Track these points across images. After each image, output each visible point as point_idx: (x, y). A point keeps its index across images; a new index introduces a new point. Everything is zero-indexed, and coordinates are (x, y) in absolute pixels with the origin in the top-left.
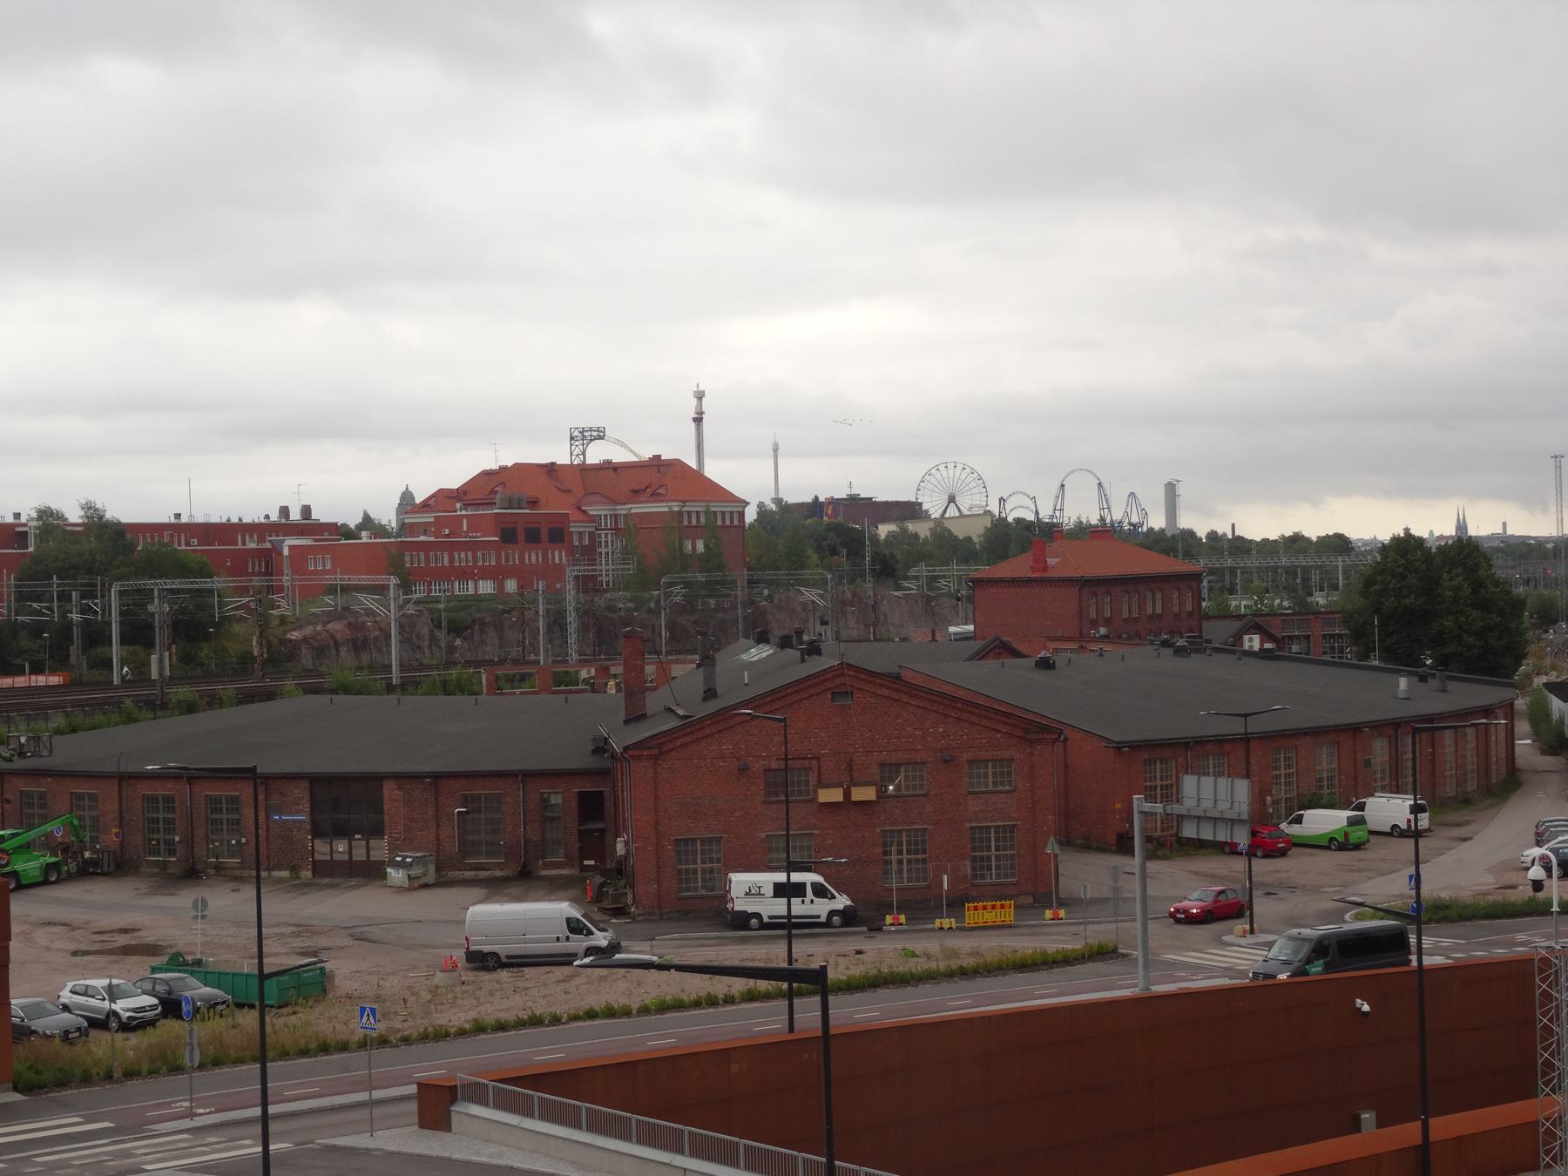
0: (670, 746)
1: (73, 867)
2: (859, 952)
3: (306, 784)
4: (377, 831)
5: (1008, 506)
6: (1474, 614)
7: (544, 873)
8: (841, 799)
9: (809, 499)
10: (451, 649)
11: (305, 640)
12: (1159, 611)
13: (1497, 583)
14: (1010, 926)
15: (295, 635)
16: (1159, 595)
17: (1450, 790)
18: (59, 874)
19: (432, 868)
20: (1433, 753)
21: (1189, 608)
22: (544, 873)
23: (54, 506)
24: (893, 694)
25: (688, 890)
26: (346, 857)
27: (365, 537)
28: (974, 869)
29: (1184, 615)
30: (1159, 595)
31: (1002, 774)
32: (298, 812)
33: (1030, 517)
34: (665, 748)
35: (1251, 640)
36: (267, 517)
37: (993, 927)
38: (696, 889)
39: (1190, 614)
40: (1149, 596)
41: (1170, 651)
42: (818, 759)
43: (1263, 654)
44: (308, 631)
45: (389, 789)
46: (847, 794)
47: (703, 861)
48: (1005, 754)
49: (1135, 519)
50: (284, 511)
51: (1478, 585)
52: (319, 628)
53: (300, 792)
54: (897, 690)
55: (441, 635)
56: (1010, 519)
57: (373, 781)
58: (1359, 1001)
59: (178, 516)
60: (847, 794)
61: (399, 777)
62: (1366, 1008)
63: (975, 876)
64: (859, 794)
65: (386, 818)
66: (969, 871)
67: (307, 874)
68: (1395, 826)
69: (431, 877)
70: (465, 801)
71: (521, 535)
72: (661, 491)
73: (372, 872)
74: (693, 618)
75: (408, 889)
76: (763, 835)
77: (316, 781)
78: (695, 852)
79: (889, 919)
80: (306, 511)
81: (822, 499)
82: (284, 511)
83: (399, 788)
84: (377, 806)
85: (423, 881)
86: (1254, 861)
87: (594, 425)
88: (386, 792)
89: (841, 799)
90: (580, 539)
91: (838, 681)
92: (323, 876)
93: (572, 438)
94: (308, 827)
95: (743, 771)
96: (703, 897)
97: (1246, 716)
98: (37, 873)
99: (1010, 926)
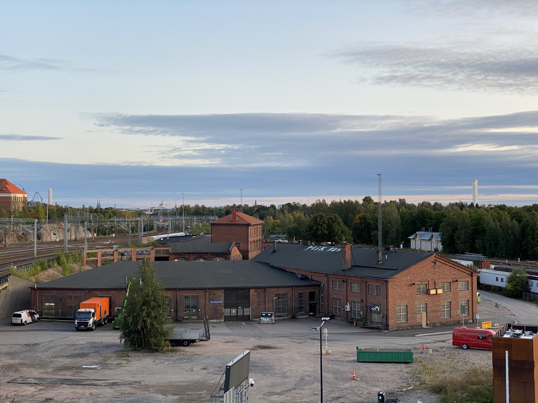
3: (223, 291)
32: (220, 300)
45: (252, 292)
53: (221, 294)
70: (277, 295)
83: (256, 291)
84: (248, 297)
88: (251, 293)
94: (223, 305)
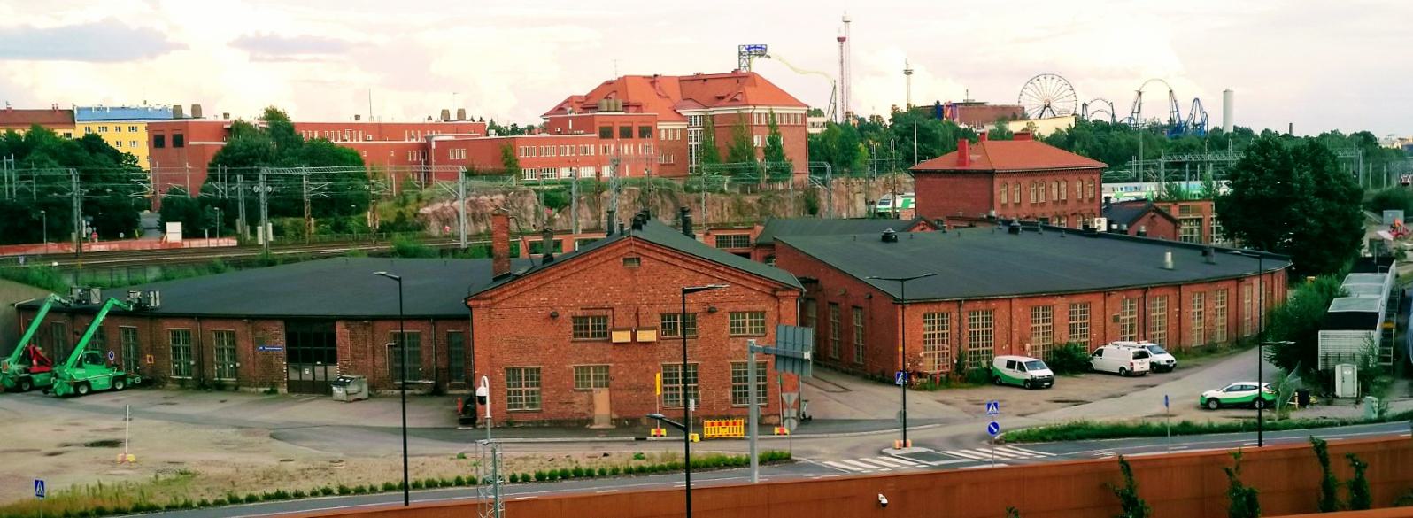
0: (500, 298)
1: (138, 380)
2: (605, 455)
4: (331, 359)
5: (1090, 109)
6: (1317, 201)
7: (450, 392)
8: (630, 340)
9: (933, 104)
10: (551, 220)
11: (435, 213)
12: (1042, 200)
13: (1340, 177)
14: (741, 439)
15: (427, 210)
16: (1063, 185)
17: (1197, 341)
18: (125, 384)
19: (365, 387)
20: (1180, 312)
21: (1091, 195)
22: (450, 392)
23: (279, 109)
24: (670, 260)
25: (515, 406)
26: (311, 378)
27: (493, 135)
28: (735, 395)
29: (1086, 201)
30: (1063, 185)
31: (757, 323)
33: (1107, 119)
34: (497, 300)
35: (1099, 222)
36: (430, 118)
37: (716, 439)
38: (521, 406)
39: (1091, 200)
40: (1055, 185)
41: (1006, 228)
42: (612, 309)
43: (1109, 235)
44: (438, 206)
46: (634, 336)
47: (527, 385)
48: (758, 307)
49: (1198, 120)
50: (445, 114)
51: (1322, 178)
52: (447, 204)
54: (673, 257)
55: (544, 209)
56: (1091, 120)
57: (330, 321)
58: (881, 495)
59: (358, 117)
60: (634, 336)
61: (348, 319)
62: (884, 501)
63: (735, 401)
64: (644, 336)
65: (338, 349)
66: (730, 397)
67: (283, 390)
68: (1122, 369)
69: (365, 394)
71: (616, 132)
72: (738, 97)
73: (322, 389)
74: (758, 197)
75: (347, 402)
76: (571, 366)
77: (289, 321)
78: (520, 378)
79: (653, 432)
80: (461, 114)
81: (942, 104)
82: (445, 114)
83: (347, 327)
84: (332, 339)
85: (358, 397)
86: (909, 393)
87: (758, 43)
88: (337, 330)
89: (630, 340)
90: (667, 135)
91: (628, 250)
92: (294, 392)
93: (740, 53)
95: (554, 316)
96: (526, 412)
97: (902, 280)
98: (106, 382)
99: (741, 439)
